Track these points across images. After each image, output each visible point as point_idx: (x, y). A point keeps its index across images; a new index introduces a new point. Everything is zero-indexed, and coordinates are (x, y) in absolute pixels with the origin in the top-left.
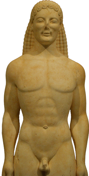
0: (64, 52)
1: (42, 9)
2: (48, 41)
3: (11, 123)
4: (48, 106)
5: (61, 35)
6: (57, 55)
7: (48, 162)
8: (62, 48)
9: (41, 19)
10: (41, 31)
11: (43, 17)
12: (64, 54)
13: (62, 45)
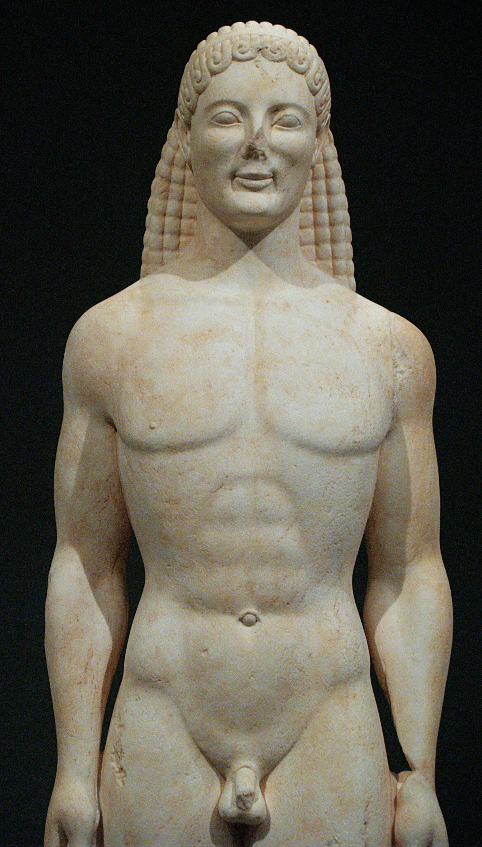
1: (234, 63)
2: (263, 214)
4: (262, 517)
6: (301, 279)
7: (263, 782)
8: (328, 247)
10: (227, 168)
11: (237, 98)
12: (335, 272)
13: (326, 231)
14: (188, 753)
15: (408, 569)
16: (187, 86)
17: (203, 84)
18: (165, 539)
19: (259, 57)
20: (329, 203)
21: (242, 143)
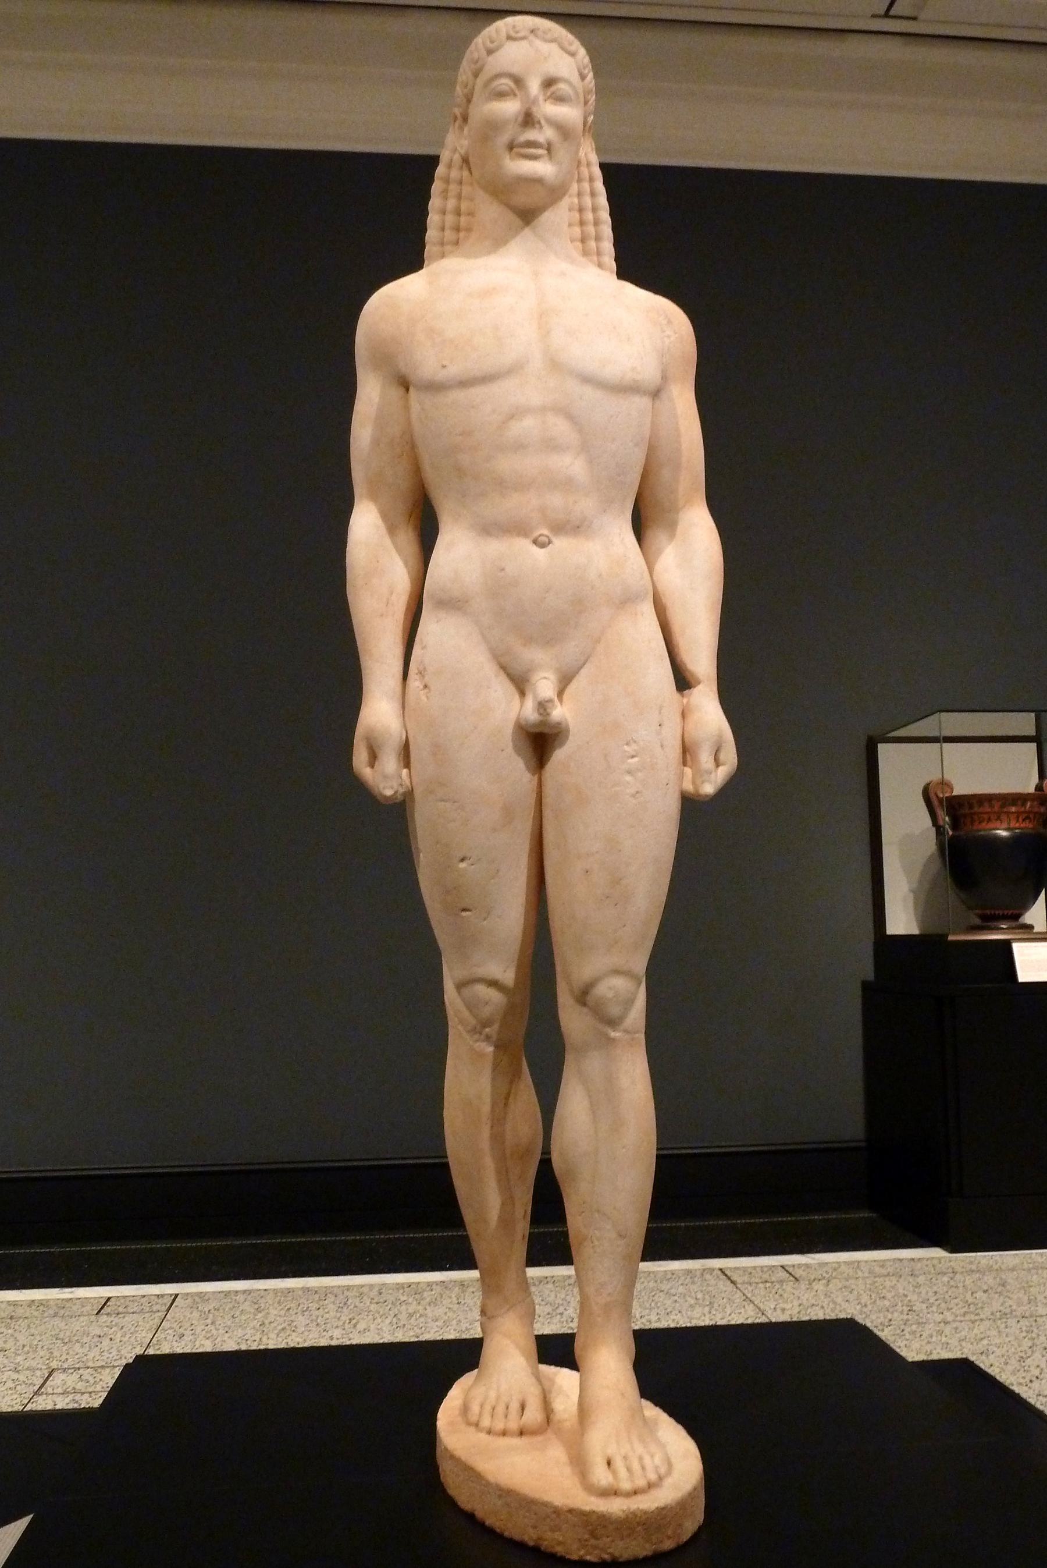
3: (387, 541)
4: (551, 445)
5: (586, 186)
6: (573, 262)
7: (560, 694)
8: (592, 244)
9: (506, 83)
10: (504, 139)
11: (515, 70)
12: (600, 265)
13: (591, 229)
14: (489, 669)
15: (681, 514)
18: (460, 471)
19: (532, 37)
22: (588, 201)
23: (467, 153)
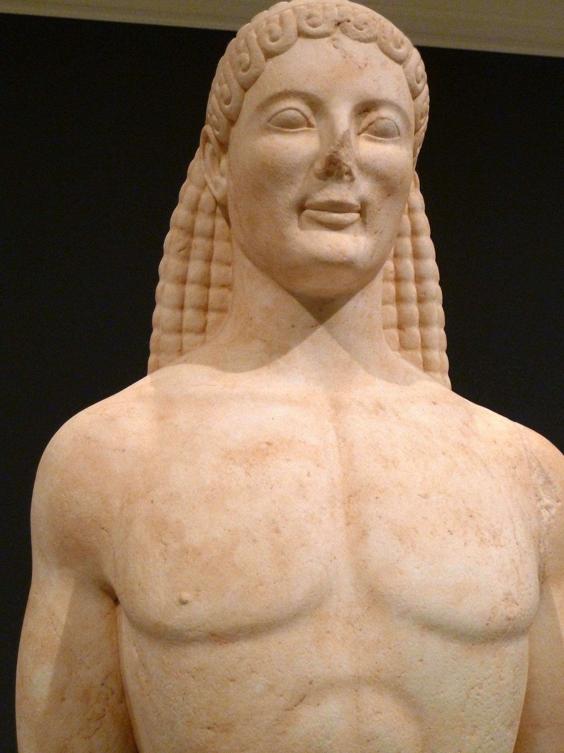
0: (425, 359)
1: (302, 42)
2: (346, 265)
6: (390, 374)
8: (415, 331)
9: (294, 107)
10: (292, 193)
11: (310, 88)
12: (426, 366)
13: (413, 309)
16: (227, 82)
17: (253, 71)
19: (338, 34)
20: (416, 269)
21: (317, 156)
22: (409, 265)
23: (225, 197)
